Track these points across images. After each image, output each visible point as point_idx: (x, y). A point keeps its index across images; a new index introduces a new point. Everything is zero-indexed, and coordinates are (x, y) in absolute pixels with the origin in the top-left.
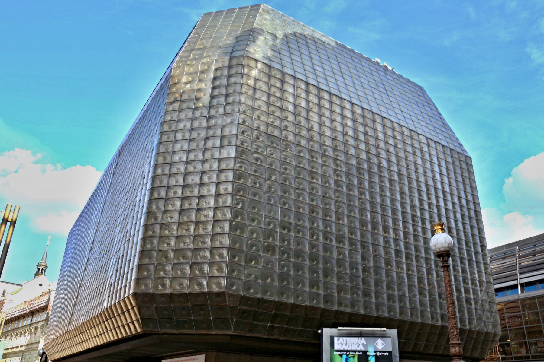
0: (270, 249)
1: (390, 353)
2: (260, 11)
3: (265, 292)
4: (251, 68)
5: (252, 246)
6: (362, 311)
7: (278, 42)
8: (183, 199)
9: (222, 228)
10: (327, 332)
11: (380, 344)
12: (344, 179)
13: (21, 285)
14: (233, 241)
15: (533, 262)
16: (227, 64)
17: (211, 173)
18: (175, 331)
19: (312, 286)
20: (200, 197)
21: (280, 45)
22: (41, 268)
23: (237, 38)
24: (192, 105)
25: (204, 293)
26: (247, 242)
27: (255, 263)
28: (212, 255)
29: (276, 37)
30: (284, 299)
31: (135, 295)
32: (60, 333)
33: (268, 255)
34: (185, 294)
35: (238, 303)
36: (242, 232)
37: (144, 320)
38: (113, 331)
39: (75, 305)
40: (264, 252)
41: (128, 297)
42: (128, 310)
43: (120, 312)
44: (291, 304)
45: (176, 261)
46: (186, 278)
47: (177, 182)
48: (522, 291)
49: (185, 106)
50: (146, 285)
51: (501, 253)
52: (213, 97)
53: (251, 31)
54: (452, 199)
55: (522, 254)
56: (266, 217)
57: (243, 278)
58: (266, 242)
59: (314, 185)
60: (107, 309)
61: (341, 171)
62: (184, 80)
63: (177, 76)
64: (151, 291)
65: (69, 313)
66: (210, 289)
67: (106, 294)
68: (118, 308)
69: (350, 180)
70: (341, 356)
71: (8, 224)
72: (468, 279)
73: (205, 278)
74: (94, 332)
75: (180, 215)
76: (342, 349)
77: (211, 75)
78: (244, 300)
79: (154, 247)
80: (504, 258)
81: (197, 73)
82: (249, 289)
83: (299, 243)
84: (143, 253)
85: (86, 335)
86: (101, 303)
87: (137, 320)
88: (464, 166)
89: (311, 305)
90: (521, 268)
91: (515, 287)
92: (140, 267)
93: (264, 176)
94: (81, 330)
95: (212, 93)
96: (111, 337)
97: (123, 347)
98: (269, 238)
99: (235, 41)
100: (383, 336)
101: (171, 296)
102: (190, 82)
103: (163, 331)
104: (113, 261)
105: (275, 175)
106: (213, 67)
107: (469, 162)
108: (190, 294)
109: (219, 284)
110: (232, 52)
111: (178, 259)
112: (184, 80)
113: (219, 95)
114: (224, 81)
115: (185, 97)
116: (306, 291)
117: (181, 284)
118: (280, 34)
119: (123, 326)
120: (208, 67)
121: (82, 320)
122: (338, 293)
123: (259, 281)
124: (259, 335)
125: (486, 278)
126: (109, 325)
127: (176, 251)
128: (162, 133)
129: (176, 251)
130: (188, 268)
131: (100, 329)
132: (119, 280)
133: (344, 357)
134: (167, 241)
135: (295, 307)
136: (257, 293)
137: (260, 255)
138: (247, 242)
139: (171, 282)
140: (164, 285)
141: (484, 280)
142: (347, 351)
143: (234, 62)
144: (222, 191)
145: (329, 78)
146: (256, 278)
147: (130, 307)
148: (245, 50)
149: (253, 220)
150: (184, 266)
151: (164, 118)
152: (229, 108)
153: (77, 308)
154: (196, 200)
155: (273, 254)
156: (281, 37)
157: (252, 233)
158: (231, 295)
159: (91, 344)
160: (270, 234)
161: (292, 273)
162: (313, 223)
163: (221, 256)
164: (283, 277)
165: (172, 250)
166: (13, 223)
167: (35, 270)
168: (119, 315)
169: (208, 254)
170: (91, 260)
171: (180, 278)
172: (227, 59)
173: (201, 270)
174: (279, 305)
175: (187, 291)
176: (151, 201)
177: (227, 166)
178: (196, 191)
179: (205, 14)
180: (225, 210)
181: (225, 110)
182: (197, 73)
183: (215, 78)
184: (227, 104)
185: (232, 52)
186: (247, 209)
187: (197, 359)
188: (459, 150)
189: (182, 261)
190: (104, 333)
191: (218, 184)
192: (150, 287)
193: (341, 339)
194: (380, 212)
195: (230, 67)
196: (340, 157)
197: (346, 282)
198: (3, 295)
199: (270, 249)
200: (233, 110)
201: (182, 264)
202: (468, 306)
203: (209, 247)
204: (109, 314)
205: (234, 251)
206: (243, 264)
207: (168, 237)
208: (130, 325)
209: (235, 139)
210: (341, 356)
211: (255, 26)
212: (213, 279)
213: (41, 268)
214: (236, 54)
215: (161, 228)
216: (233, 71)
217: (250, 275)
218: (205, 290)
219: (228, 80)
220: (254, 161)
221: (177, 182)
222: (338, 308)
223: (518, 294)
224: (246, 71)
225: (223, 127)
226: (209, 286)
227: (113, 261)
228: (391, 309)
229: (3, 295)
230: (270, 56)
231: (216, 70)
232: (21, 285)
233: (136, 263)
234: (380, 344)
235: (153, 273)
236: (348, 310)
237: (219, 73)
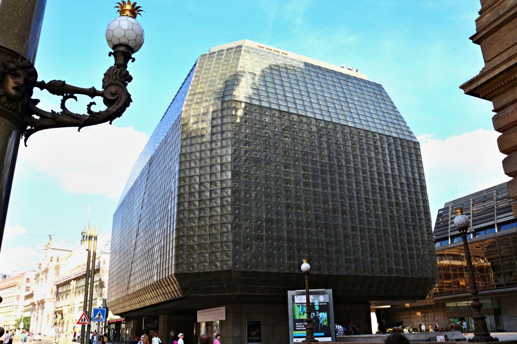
0: (259, 238)
1: (328, 303)
2: (243, 52)
3: (257, 266)
4: (236, 109)
5: (247, 238)
6: (326, 273)
7: (257, 78)
8: (200, 210)
9: (227, 228)
10: (290, 293)
11: (322, 298)
13: (71, 251)
14: (235, 236)
15: (508, 204)
16: (220, 108)
18: (203, 295)
19: (289, 259)
20: (211, 208)
21: (259, 82)
22: (85, 235)
23: (226, 82)
24: (199, 140)
25: (219, 271)
26: (244, 235)
27: (250, 249)
28: (222, 246)
29: (255, 75)
31: (175, 274)
32: (121, 295)
34: (207, 272)
36: (239, 230)
37: (183, 289)
38: (163, 295)
39: (130, 276)
40: (255, 241)
41: (171, 276)
42: (172, 283)
43: (167, 284)
44: (275, 272)
45: (199, 252)
46: (207, 262)
47: (195, 172)
48: (499, 230)
49: (194, 141)
50: (182, 268)
51: (482, 197)
52: (212, 134)
53: (236, 75)
54: (400, 180)
55: (499, 197)
57: (242, 259)
59: (288, 189)
60: (157, 281)
61: (309, 175)
62: (192, 121)
63: (186, 118)
64: (186, 271)
65: (126, 281)
67: (155, 271)
68: (165, 282)
70: (299, 306)
71: (93, 238)
72: (412, 241)
73: (218, 261)
74: (148, 296)
75: (199, 220)
76: (299, 302)
77: (210, 117)
78: (244, 273)
79: (185, 243)
80: (484, 202)
81: (199, 115)
82: (247, 265)
83: (279, 230)
84: (178, 247)
85: (142, 298)
86: (152, 277)
87: (179, 290)
88: (413, 151)
89: (289, 272)
90: (498, 210)
91: (493, 226)
92: (177, 257)
94: (137, 294)
95: (212, 131)
96: (161, 299)
97: (170, 305)
98: (258, 230)
99: (224, 86)
100: (323, 293)
101: (198, 274)
102: (196, 123)
103: (196, 295)
104: (156, 248)
105: (260, 186)
106: (211, 110)
107: (417, 147)
108: (210, 272)
109: (227, 265)
110: (223, 97)
111: (201, 250)
112: (192, 121)
113: (217, 133)
114: (219, 121)
115: (193, 134)
116: (285, 263)
117: (204, 266)
118: (258, 72)
119: (170, 293)
120: (208, 110)
121: (138, 288)
123: (253, 260)
124: (256, 294)
125: (428, 238)
126: (160, 291)
127: (199, 245)
128: (181, 163)
129: (199, 245)
130: (207, 255)
131: (153, 294)
132: (163, 263)
133: (301, 307)
134: (192, 238)
135: (278, 274)
136: (252, 268)
137: (253, 244)
138: (244, 235)
139: (198, 265)
140: (193, 267)
141: (426, 239)
142: (302, 303)
143: (225, 105)
144: (225, 203)
145: (297, 101)
146: (251, 258)
147: (173, 282)
148: (232, 94)
149: (246, 220)
150: (205, 254)
151: (181, 151)
152: (224, 142)
153: (132, 278)
154: (209, 210)
155: (262, 241)
156: (259, 73)
157: (246, 229)
158: (235, 271)
159: (147, 303)
160: (259, 228)
161: (275, 252)
162: (289, 216)
163: (228, 246)
164: (270, 256)
165: (196, 244)
166: (96, 238)
167: (81, 238)
168: (166, 286)
169: (219, 245)
170: (139, 243)
171: (203, 262)
172: (219, 103)
173: (216, 256)
174: (267, 274)
175: (208, 270)
176: (179, 212)
179: (202, 56)
180: (228, 216)
181: (221, 144)
182: (199, 115)
183: (213, 119)
184: (223, 139)
185: (223, 97)
186: (242, 213)
187: (220, 309)
188: (408, 138)
189: (203, 251)
190: (156, 297)
191: (222, 198)
192: (184, 269)
193: (299, 297)
194: (347, 194)
195: (222, 110)
198: (58, 260)
199: (259, 238)
200: (227, 144)
201: (203, 253)
202: (412, 260)
203: (219, 241)
204: (159, 285)
205: (235, 243)
206: (242, 250)
208: (173, 291)
210: (299, 306)
211: (239, 69)
212: (223, 261)
213: (85, 235)
214: (227, 99)
215: (187, 230)
216: (225, 113)
217: (247, 257)
218: (220, 269)
219: (222, 121)
223: (495, 232)
224: (234, 112)
225: (221, 157)
226: (221, 267)
227: (156, 248)
228: (347, 269)
229: (58, 260)
230: (251, 94)
231: (213, 112)
232: (71, 251)
233: (174, 254)
234: (322, 298)
235: (186, 259)
237: (215, 116)
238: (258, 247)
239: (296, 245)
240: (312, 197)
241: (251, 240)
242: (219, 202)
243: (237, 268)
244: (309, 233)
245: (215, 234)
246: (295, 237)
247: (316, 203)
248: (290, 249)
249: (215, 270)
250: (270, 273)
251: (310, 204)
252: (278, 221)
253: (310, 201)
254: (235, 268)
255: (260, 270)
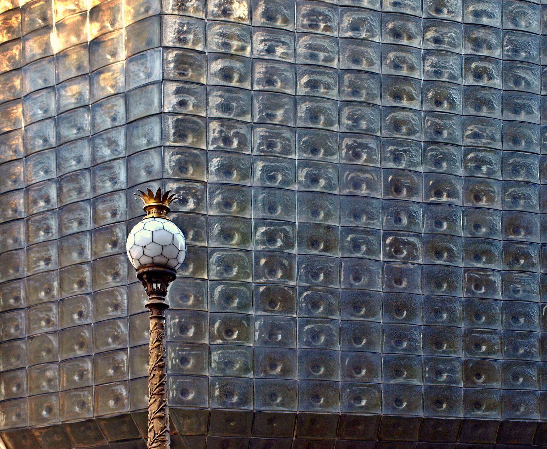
0: (273, 297)
12: (497, 82)
17: (113, 134)
26: (343, 361)
30: (319, 408)
33: (277, 314)
35: (203, 428)
44: (336, 415)
56: (260, 222)
58: (262, 284)
66: (135, 405)
69: (517, 80)
89: (390, 413)
93: (248, 118)
122: (467, 379)
127: (60, 333)
129: (60, 333)
135: (348, 423)
137: (248, 318)
169: (123, 328)
177: (147, 109)
178: (87, 182)
196: (490, 16)
197: (494, 353)
207: (78, 299)
209: (157, 27)
220: (390, 40)
221: (79, 160)
222: (465, 414)
236: (496, 416)
238: (271, 329)
239: (420, 322)
240: (498, 146)
241: (243, 306)
242: (122, 176)
243: (190, 403)
244: (479, 281)
245: (111, 293)
246: (421, 292)
247: (516, 170)
248: (396, 336)
249: (116, 413)
250: (315, 419)
251: (491, 172)
252: (360, 238)
253: (489, 163)
254: (182, 402)
255: (277, 407)
